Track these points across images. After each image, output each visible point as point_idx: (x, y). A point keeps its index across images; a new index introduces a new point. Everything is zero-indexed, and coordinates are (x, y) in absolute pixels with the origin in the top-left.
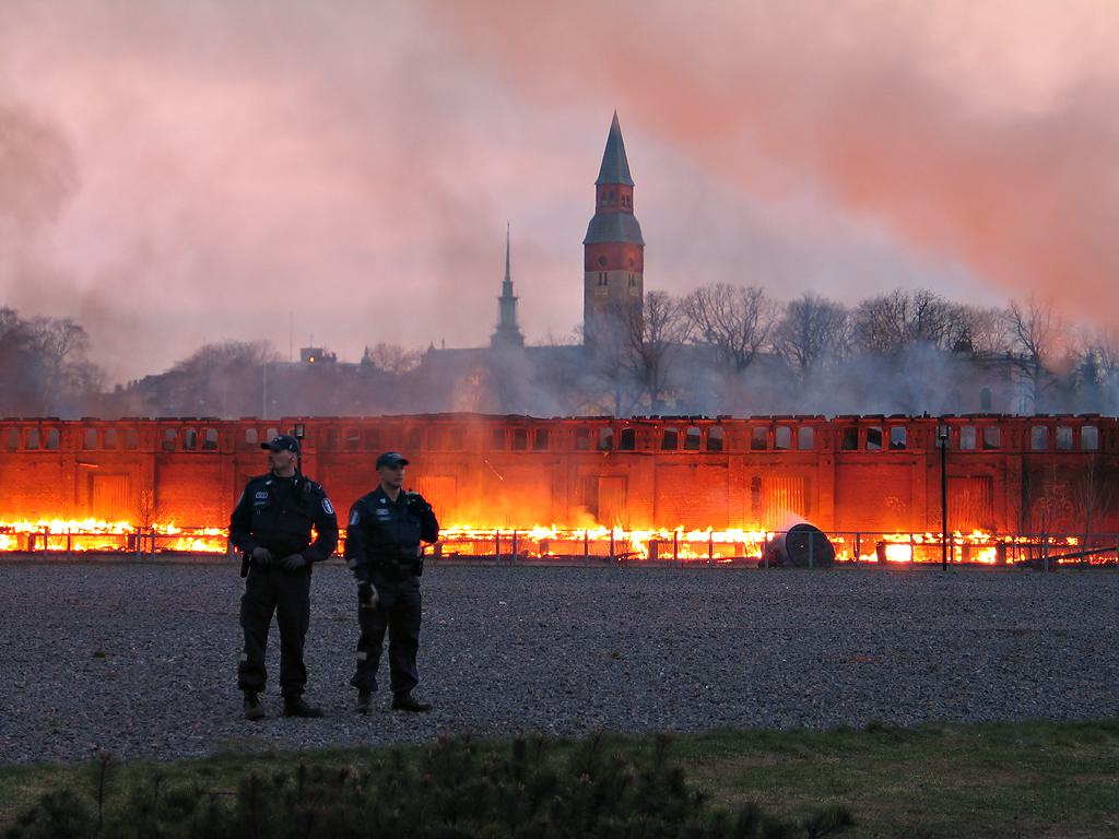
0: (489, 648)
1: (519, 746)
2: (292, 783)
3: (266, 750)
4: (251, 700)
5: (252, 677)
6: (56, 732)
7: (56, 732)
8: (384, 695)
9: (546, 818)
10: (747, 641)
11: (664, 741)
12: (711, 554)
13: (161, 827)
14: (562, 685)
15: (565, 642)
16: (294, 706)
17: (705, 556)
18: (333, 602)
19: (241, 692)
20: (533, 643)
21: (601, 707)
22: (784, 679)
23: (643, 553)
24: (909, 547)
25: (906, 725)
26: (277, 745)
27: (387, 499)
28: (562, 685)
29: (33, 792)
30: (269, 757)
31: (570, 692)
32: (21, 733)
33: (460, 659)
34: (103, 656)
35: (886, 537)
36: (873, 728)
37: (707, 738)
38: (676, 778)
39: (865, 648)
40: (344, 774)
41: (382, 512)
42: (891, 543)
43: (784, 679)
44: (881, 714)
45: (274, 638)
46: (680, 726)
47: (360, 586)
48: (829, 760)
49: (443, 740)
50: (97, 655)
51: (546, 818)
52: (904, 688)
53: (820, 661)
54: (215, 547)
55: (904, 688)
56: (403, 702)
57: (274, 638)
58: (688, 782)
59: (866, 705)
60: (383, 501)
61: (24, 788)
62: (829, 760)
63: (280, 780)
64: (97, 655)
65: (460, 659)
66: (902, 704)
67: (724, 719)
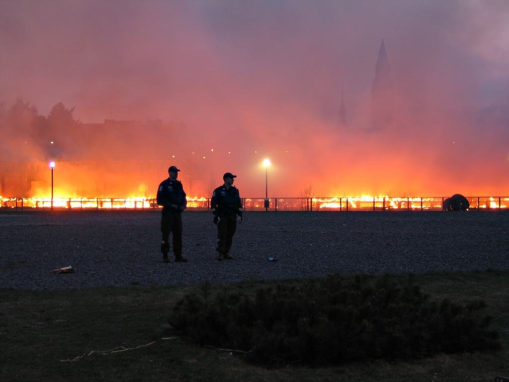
0: (340, 242)
1: (357, 278)
2: (274, 292)
3: (262, 279)
4: (165, 256)
5: (165, 249)
6: (185, 273)
7: (185, 273)
8: (171, 254)
9: (369, 304)
10: (438, 238)
11: (412, 275)
12: (422, 206)
13: (229, 307)
14: (369, 255)
15: (369, 239)
16: (179, 259)
17: (419, 207)
18: (281, 226)
19: (162, 253)
20: (357, 240)
21: (384, 263)
22: (453, 253)
23: (395, 207)
24: (373, 201)
25: (501, 269)
26: (265, 278)
27: (226, 189)
28: (369, 255)
29: (180, 294)
30: (263, 282)
31: (372, 258)
32: (174, 273)
33: (330, 246)
34: (200, 245)
35: (103, 200)
36: (489, 271)
37: (425, 275)
38: (416, 290)
39: (484, 241)
40: (293, 288)
41: (223, 192)
42: (105, 201)
43: (453, 253)
44: (492, 266)
45: (171, 237)
46: (414, 270)
47: (215, 217)
48: (473, 283)
49: (329, 275)
50: (198, 245)
51: (369, 304)
52: (500, 256)
53: (467, 245)
54: (440, 206)
55: (500, 256)
56: (179, 259)
57: (171, 237)
58: (422, 291)
59: (486, 262)
60: (224, 189)
61: (176, 292)
62: (473, 283)
63: (269, 290)
64: (198, 245)
65: (330, 246)
66: (500, 262)
67: (431, 267)
